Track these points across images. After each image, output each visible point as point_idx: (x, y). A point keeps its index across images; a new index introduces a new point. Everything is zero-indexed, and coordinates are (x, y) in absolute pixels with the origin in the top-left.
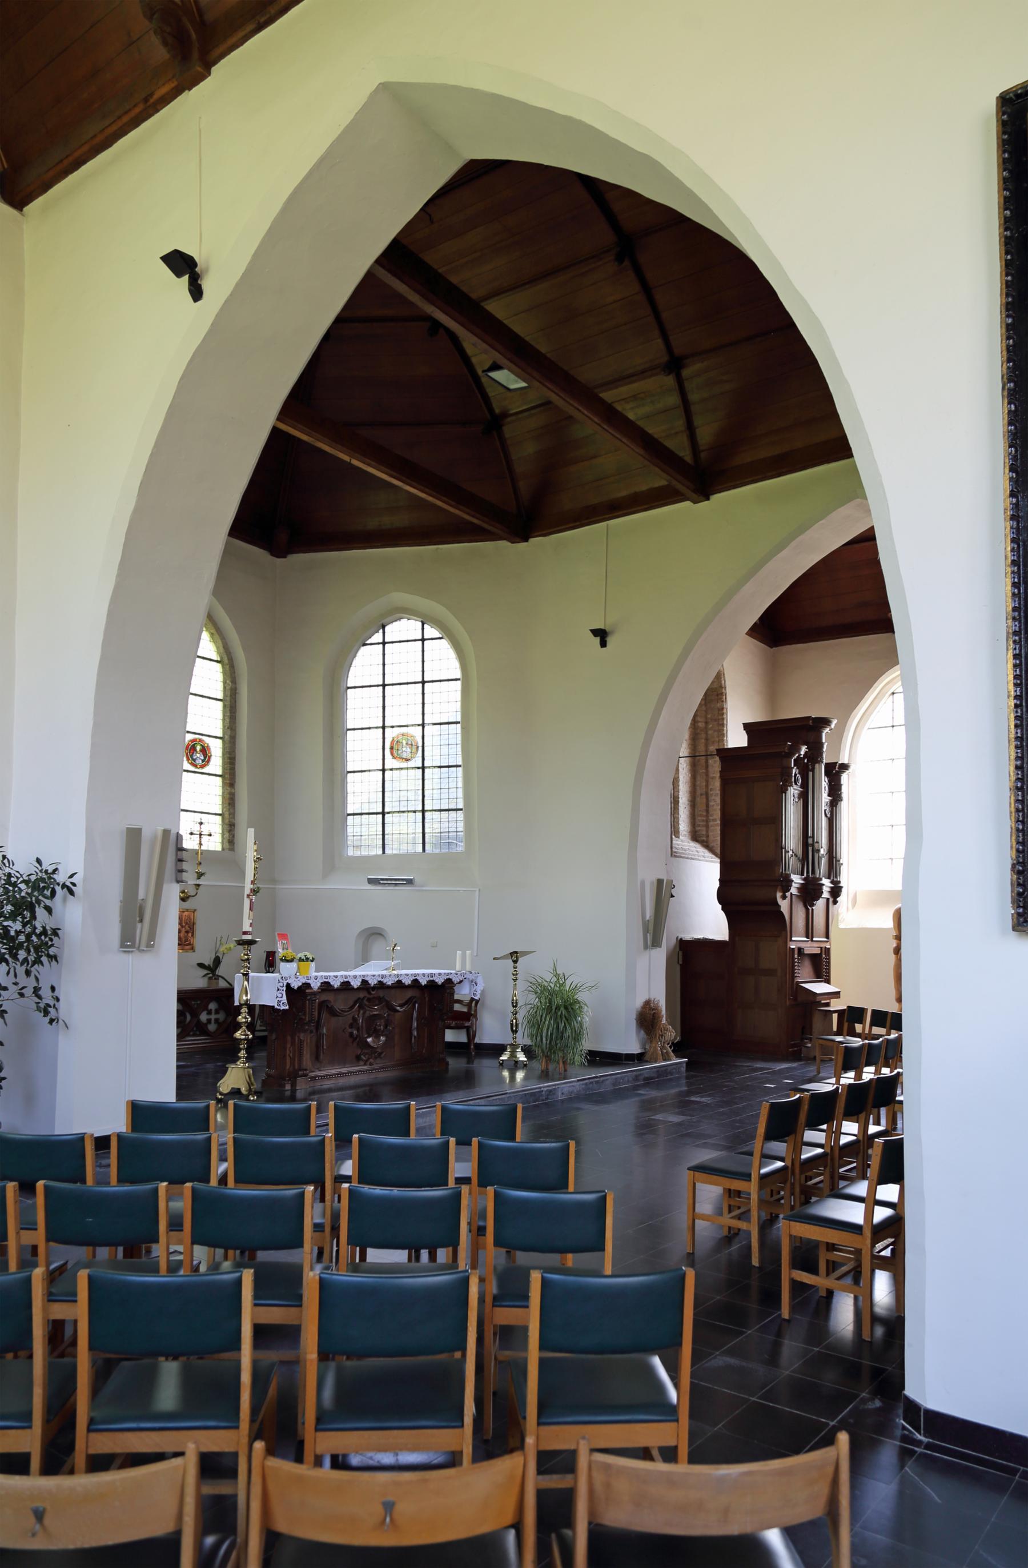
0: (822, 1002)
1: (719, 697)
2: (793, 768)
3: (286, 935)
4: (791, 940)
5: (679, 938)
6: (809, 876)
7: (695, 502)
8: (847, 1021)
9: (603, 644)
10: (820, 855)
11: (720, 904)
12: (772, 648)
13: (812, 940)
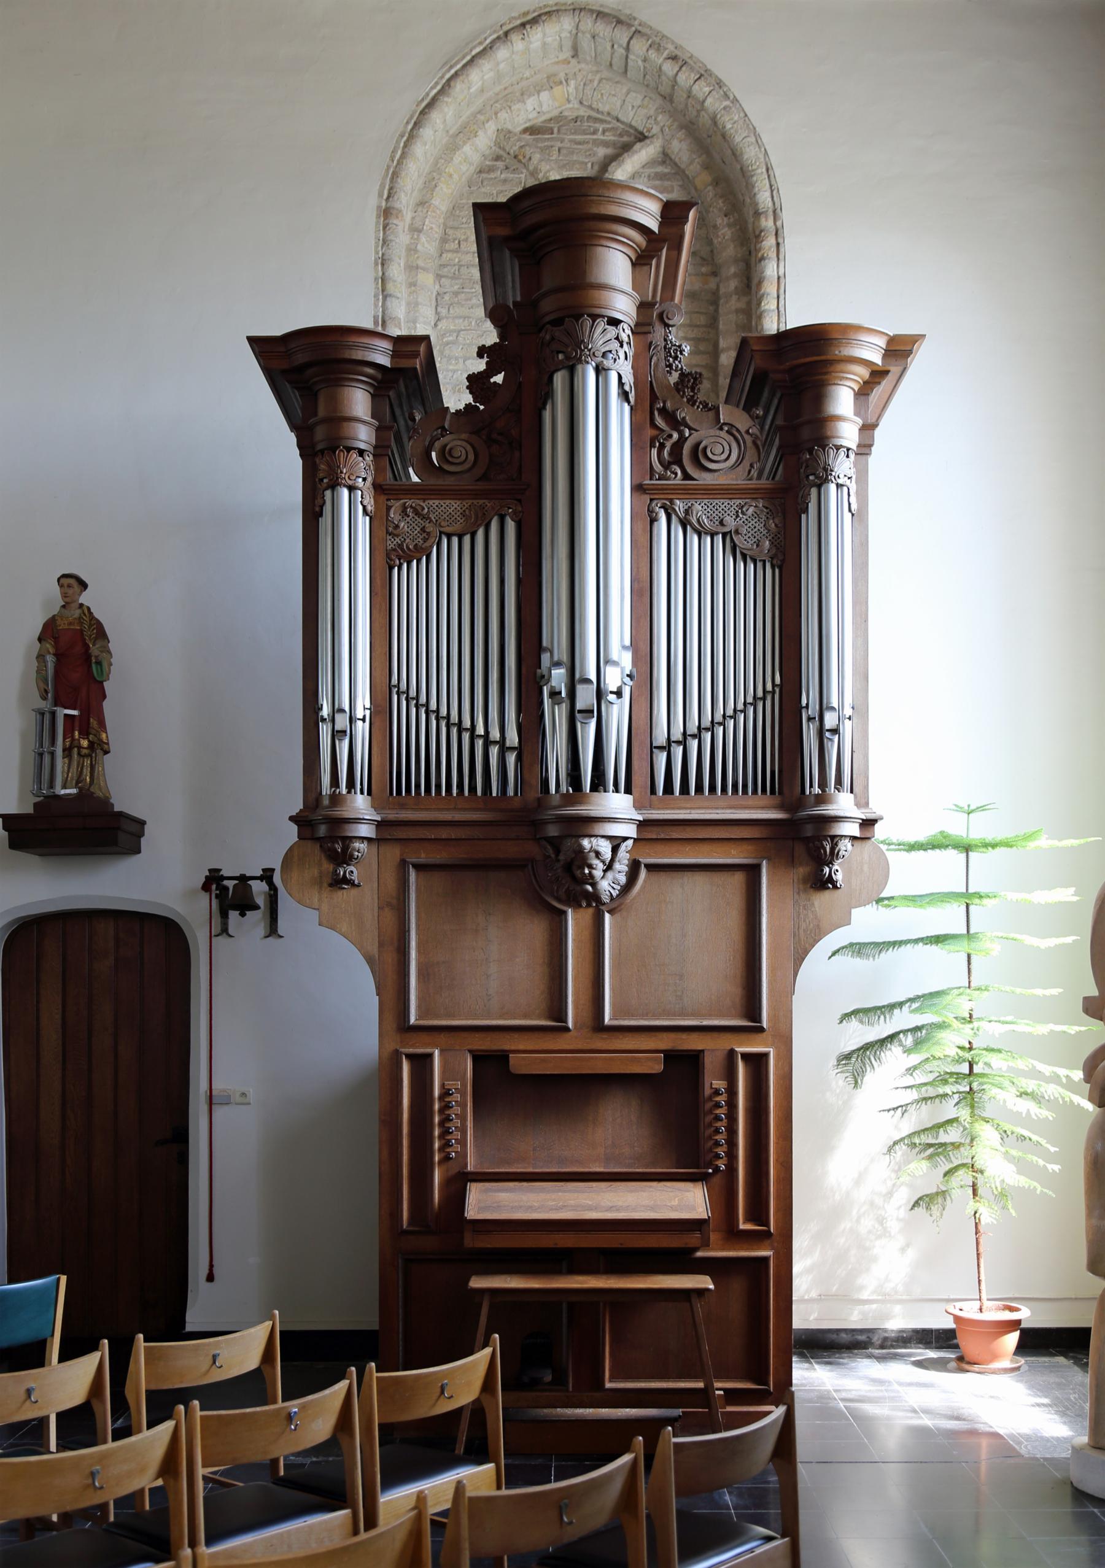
0: (699, 1254)
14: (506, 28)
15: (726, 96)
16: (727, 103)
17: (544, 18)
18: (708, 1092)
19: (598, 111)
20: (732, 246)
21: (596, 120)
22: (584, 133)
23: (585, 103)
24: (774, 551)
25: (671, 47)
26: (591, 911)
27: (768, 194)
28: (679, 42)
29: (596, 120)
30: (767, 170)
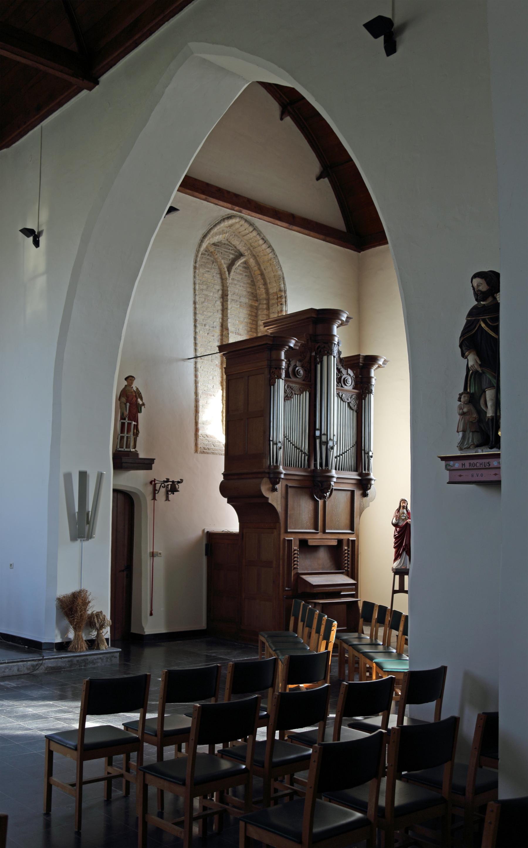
0: (342, 593)
1: (279, 300)
2: (283, 360)
3: (89, 536)
4: (286, 532)
5: (206, 531)
6: (317, 468)
7: (90, 89)
8: (302, 621)
9: (36, 243)
10: (329, 448)
11: (224, 496)
12: (360, 252)
13: (324, 532)
14: (224, 217)
15: (274, 254)
16: (275, 256)
17: (233, 217)
18: (344, 550)
19: (231, 243)
20: (265, 295)
21: (229, 246)
22: (227, 249)
23: (229, 240)
24: (357, 409)
25: (262, 235)
26: (323, 500)
27: (283, 285)
28: (265, 235)
29: (229, 246)
30: (283, 278)
